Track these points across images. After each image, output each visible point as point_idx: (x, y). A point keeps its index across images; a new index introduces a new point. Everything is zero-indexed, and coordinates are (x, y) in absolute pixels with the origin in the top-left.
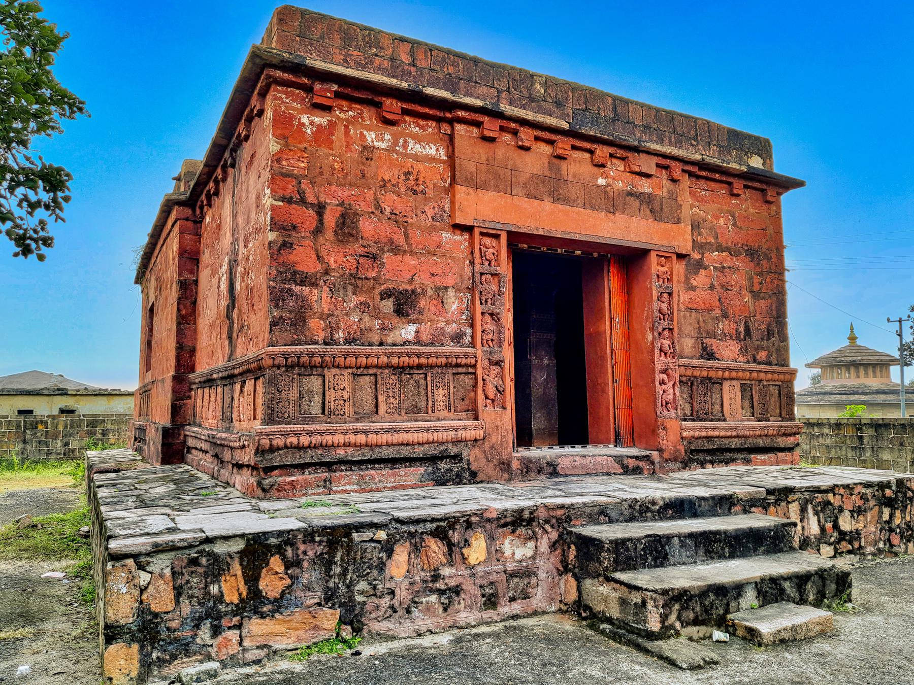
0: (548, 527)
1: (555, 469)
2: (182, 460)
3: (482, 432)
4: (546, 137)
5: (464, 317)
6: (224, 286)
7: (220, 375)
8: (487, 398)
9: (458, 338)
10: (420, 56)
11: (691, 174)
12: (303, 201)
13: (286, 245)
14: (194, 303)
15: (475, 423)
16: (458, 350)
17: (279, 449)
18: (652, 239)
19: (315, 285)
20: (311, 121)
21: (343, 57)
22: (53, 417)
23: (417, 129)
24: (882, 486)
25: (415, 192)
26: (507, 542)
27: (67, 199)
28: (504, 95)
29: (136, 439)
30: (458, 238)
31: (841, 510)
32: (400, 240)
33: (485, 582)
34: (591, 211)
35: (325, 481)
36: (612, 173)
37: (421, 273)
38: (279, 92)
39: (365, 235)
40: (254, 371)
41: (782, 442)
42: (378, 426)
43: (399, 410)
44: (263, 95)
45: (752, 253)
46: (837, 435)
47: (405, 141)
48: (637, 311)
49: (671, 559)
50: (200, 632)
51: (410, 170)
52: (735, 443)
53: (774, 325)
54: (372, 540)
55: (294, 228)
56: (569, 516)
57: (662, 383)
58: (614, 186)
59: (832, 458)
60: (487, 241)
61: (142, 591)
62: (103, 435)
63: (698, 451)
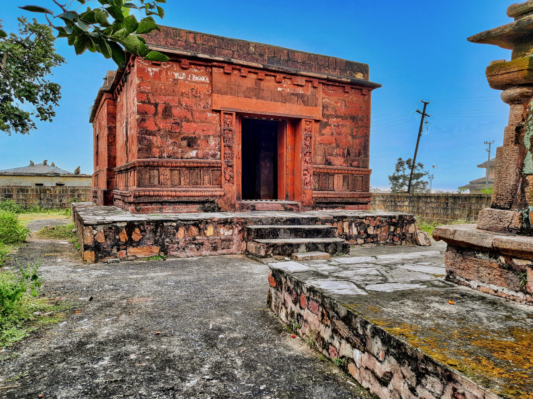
0: (237, 225)
2: (112, 204)
3: (223, 193)
5: (217, 148)
6: (124, 132)
7: (124, 169)
8: (226, 180)
9: (214, 156)
10: (198, 38)
11: (323, 84)
12: (149, 103)
13: (143, 120)
14: (115, 136)
15: (221, 189)
16: (214, 161)
17: (142, 196)
18: (303, 114)
19: (155, 135)
20: (152, 70)
21: (165, 42)
22: (54, 187)
24: (391, 217)
25: (196, 97)
26: (222, 229)
27: (60, 97)
28: (235, 53)
29: (93, 197)
30: (215, 115)
31: (369, 226)
32: (189, 116)
33: (212, 242)
35: (160, 208)
36: (285, 85)
38: (139, 59)
39: (175, 115)
40: (133, 168)
41: (361, 200)
42: (180, 189)
43: (189, 184)
44: (133, 59)
45: (353, 118)
46: (437, 202)
47: (192, 76)
48: (297, 144)
49: (280, 237)
50: (113, 250)
51: (194, 88)
52: (338, 200)
53: (362, 150)
54: (171, 226)
55: (146, 113)
56: (246, 222)
57: (305, 175)
58: (285, 91)
59: (434, 214)
60: (227, 116)
61: (95, 236)
62: (79, 197)
63: (320, 203)
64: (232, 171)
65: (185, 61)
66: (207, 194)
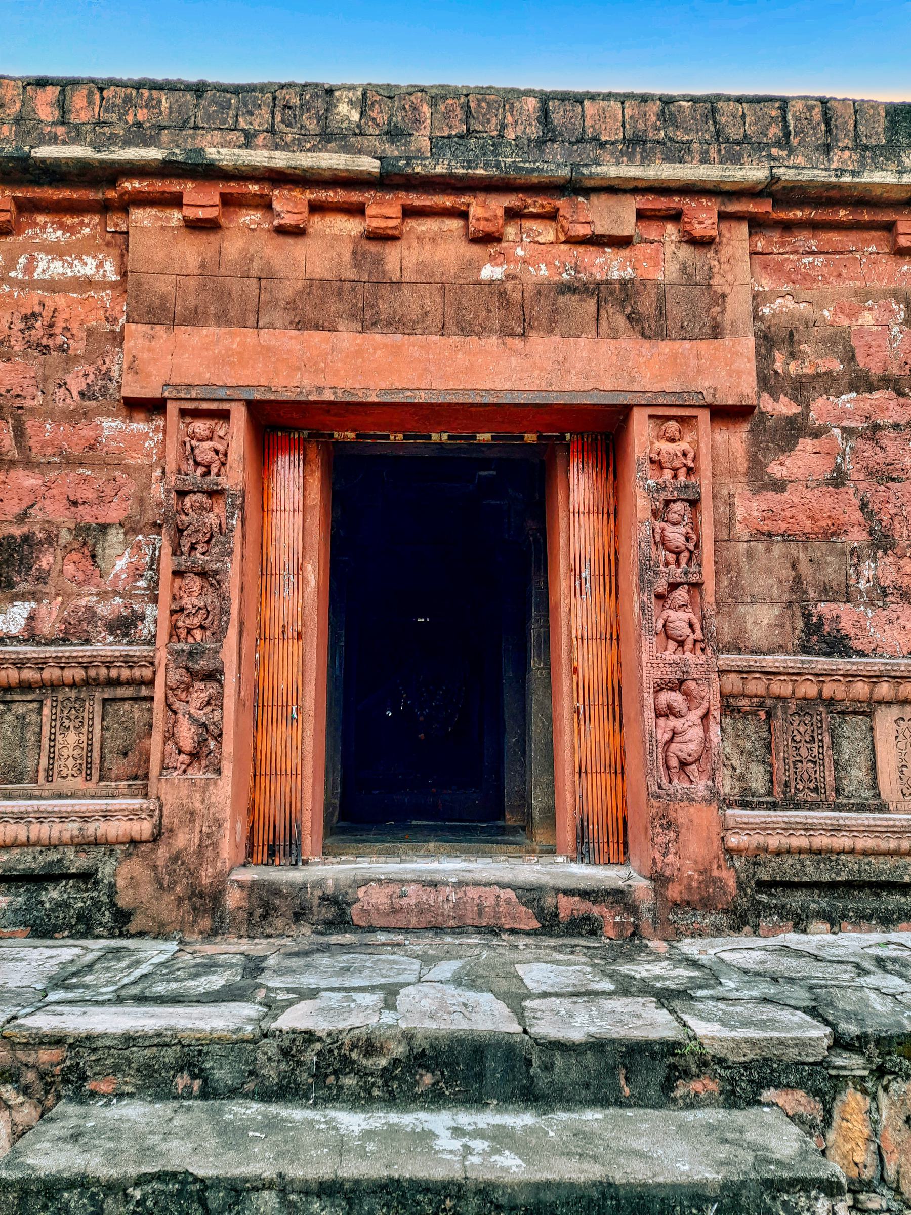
1: (342, 912)
4: (338, 198)
5: (142, 583)
11: (756, 224)
18: (633, 380)
23: (59, 233)
25: (45, 350)
30: (139, 426)
34: (462, 338)
37: (47, 502)
47: (32, 259)
51: (37, 309)
57: (670, 712)
60: (200, 426)
64: (215, 702)
66: (55, 834)
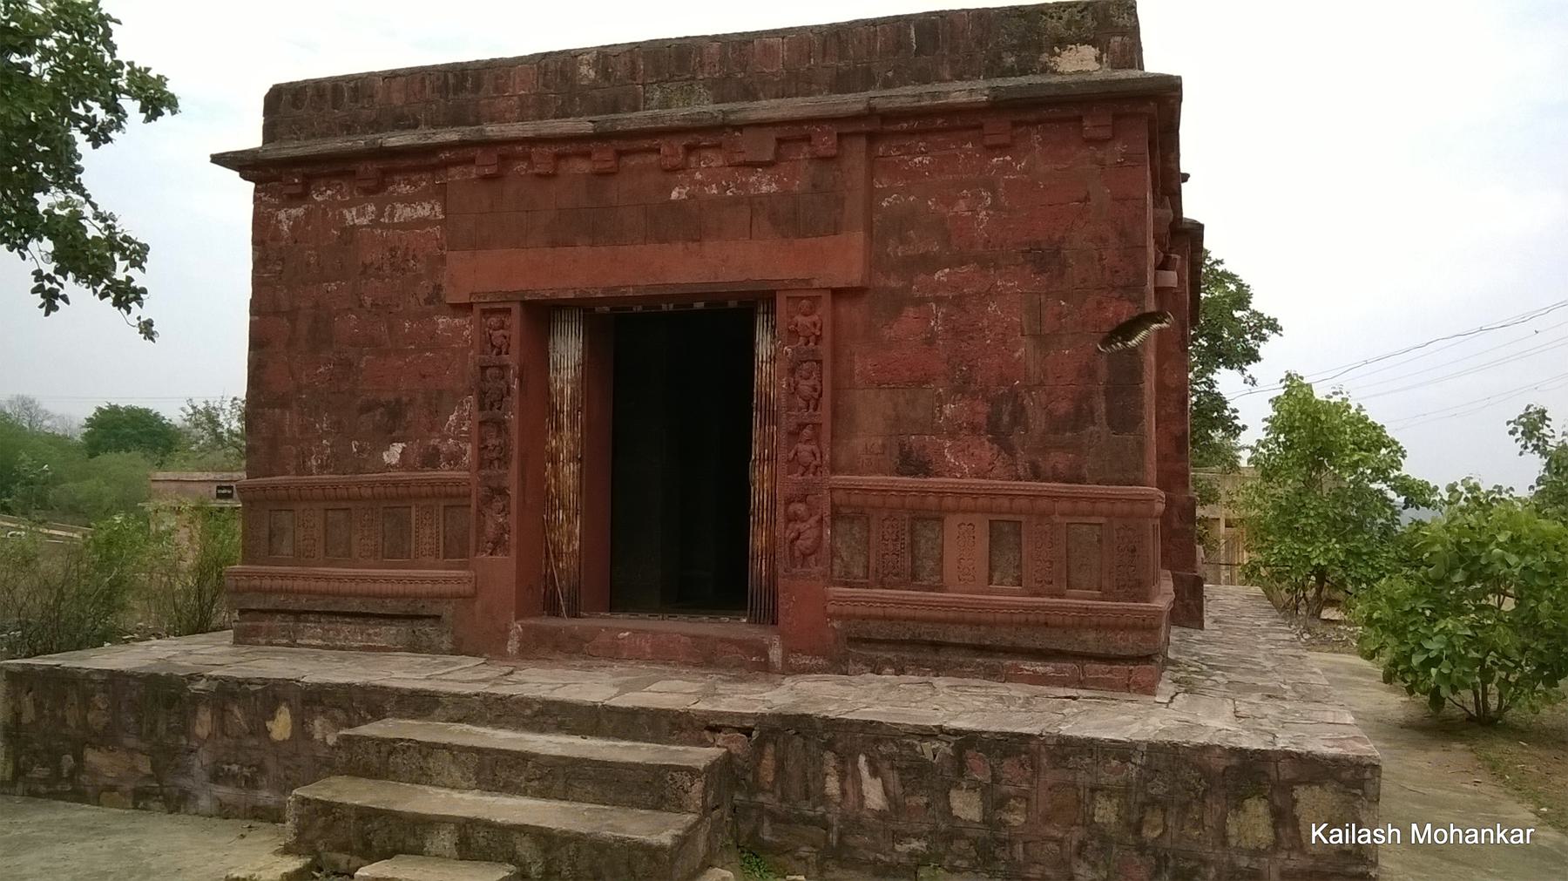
47: (393, 208)
60: (494, 320)
64: (505, 510)
65: (366, 169)
